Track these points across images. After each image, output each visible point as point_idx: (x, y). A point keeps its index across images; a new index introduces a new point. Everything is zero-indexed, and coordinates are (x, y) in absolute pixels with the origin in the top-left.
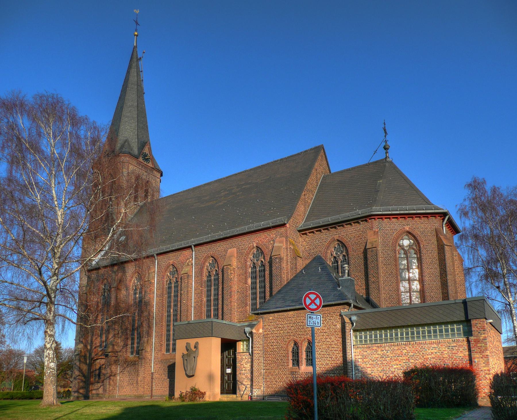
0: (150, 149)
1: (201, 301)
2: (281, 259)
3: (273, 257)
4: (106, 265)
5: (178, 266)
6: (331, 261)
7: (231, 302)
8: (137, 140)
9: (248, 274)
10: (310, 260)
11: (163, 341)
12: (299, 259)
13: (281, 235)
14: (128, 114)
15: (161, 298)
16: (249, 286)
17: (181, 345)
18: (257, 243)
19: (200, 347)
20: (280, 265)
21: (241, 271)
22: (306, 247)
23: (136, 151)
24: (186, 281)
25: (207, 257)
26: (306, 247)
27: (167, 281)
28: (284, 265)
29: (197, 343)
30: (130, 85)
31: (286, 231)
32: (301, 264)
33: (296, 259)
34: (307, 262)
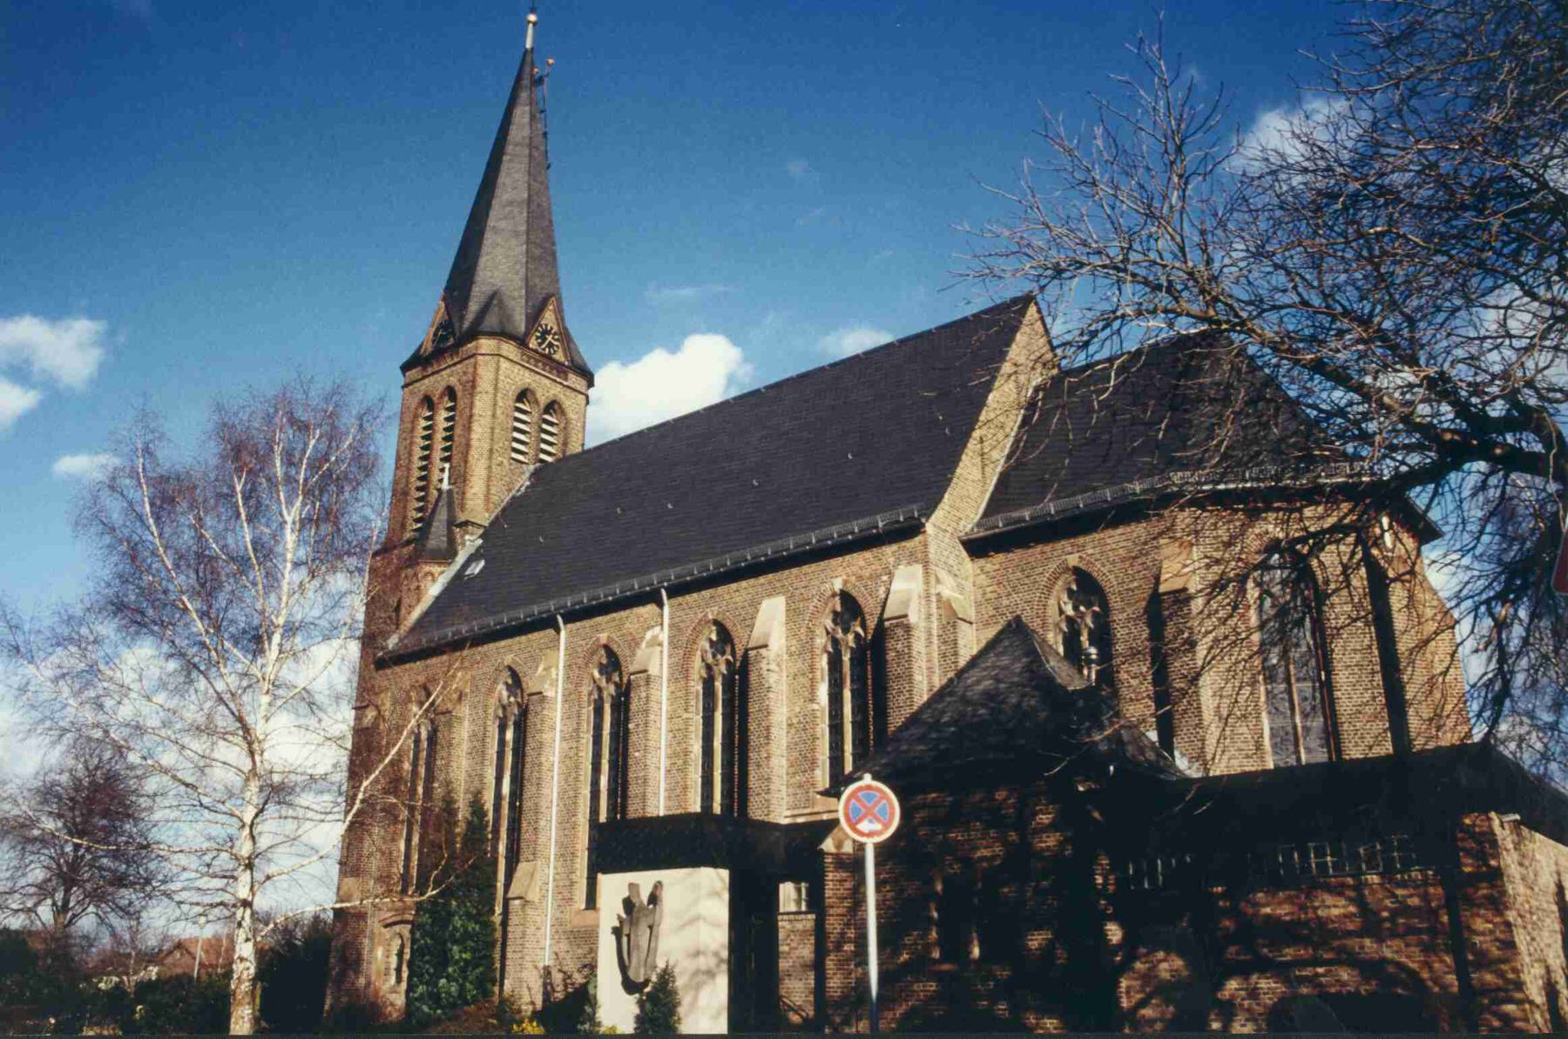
0: (559, 312)
1: (686, 753)
2: (908, 629)
3: (887, 624)
4: (397, 669)
5: (621, 650)
6: (1061, 629)
7: (768, 758)
8: (523, 292)
9: (818, 673)
10: (999, 627)
11: (578, 873)
12: (963, 626)
13: (912, 558)
14: (503, 224)
15: (575, 745)
16: (824, 708)
17: (613, 887)
18: (845, 582)
19: (669, 899)
20: (909, 647)
21: (799, 664)
22: (990, 589)
23: (520, 323)
24: (644, 694)
25: (704, 622)
26: (990, 589)
27: (590, 694)
28: (919, 645)
29: (658, 886)
30: (510, 149)
31: (926, 545)
32: (970, 642)
33: (954, 626)
34: (991, 633)
